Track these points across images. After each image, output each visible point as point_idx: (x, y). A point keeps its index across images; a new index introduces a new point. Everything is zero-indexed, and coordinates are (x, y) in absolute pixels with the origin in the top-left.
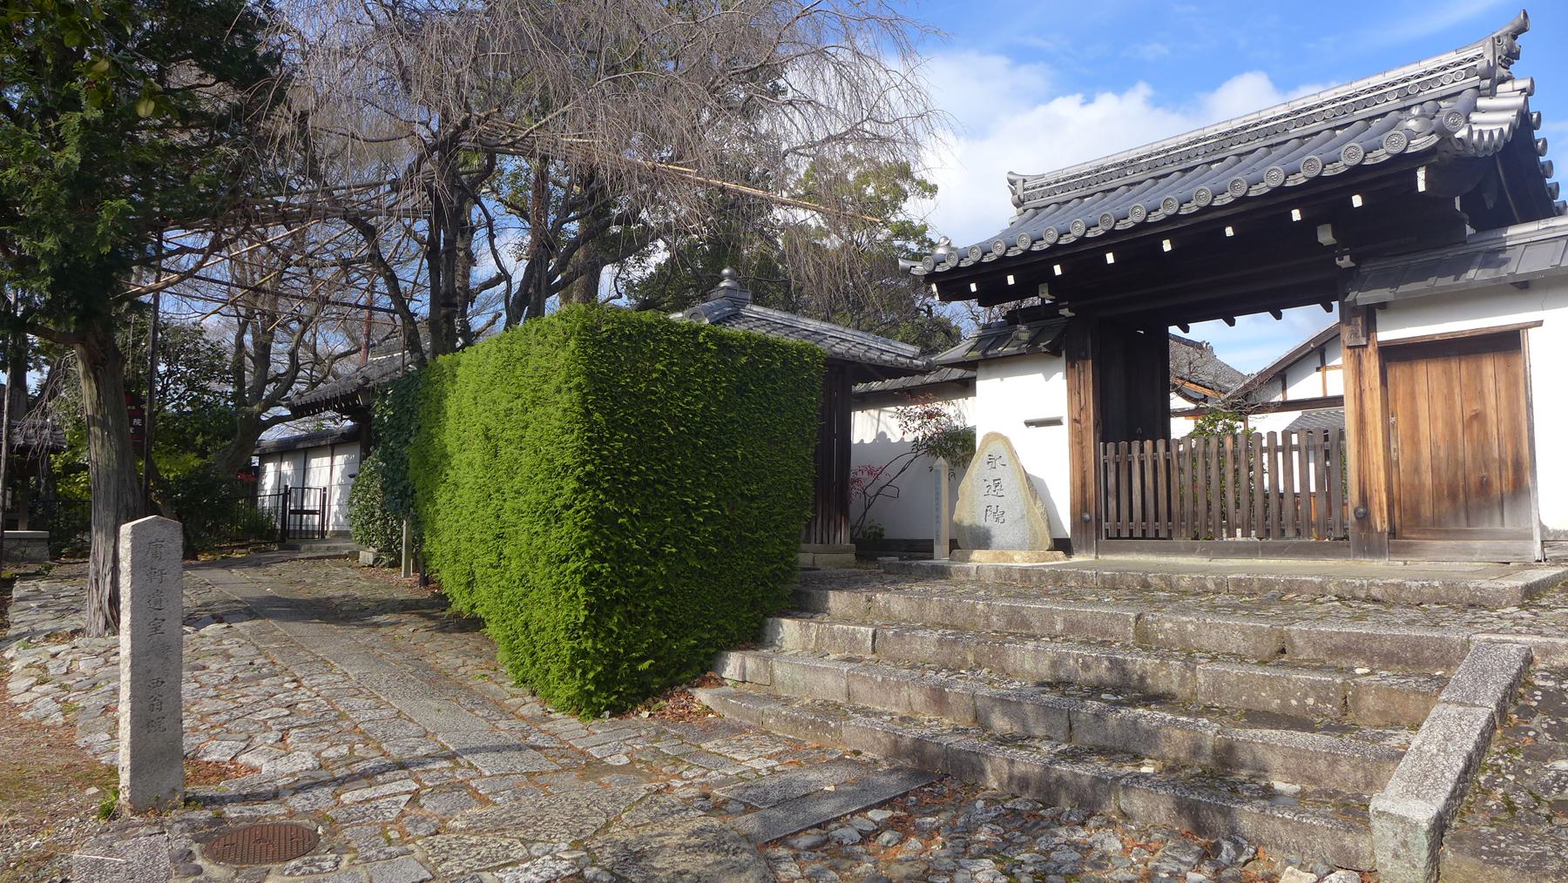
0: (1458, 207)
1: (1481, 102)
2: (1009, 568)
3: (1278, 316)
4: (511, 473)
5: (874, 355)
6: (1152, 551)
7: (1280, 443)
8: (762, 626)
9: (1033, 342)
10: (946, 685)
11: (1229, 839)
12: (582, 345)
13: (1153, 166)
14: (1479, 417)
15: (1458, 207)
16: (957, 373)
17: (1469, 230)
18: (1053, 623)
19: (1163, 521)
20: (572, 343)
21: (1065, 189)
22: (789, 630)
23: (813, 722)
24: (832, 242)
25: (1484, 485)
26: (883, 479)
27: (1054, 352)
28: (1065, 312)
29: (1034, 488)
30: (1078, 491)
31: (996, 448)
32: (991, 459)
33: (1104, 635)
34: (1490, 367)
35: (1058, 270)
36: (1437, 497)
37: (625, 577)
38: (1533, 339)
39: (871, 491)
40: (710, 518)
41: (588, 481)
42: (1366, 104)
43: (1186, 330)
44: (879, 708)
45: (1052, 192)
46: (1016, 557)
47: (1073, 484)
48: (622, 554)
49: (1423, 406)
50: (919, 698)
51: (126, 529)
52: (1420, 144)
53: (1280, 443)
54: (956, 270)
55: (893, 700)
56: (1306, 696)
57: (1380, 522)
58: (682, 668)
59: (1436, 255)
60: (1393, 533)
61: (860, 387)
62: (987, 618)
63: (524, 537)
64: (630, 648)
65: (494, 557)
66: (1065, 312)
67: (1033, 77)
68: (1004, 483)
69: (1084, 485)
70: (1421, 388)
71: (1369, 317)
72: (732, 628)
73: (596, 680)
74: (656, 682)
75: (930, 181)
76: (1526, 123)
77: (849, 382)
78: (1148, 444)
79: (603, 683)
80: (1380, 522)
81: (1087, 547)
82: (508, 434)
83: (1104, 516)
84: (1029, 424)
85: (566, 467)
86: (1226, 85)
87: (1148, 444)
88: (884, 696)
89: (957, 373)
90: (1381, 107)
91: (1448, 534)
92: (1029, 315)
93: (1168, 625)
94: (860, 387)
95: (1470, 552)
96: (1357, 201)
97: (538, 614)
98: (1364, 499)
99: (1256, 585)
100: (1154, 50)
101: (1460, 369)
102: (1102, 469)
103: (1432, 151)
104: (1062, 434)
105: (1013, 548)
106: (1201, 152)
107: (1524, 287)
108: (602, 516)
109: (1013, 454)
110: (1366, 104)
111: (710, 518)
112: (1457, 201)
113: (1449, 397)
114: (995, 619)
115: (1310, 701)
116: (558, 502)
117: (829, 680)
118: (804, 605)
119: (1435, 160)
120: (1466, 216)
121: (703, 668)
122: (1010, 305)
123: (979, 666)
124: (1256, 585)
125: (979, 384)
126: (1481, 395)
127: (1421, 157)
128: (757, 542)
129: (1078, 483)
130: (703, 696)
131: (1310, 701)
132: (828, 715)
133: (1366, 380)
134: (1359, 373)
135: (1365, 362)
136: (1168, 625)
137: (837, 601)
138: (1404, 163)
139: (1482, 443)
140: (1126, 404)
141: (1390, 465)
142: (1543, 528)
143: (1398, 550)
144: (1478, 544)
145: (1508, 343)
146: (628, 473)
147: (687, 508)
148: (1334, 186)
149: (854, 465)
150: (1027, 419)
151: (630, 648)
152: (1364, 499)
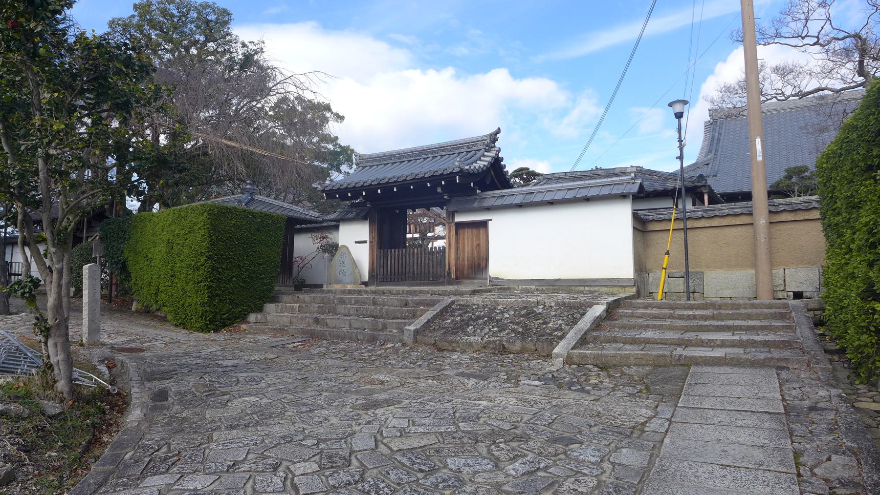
1: (486, 154)
4: (179, 255)
5: (303, 216)
6: (393, 285)
8: (262, 306)
9: (357, 215)
12: (209, 214)
13: (400, 158)
14: (479, 245)
16: (334, 223)
19: (399, 276)
20: (205, 214)
21: (373, 161)
22: (270, 307)
24: (289, 142)
25: (479, 265)
26: (306, 261)
27: (364, 218)
29: (354, 264)
31: (343, 250)
32: (342, 254)
34: (482, 231)
35: (443, 183)
36: (468, 268)
37: (220, 288)
38: (490, 224)
39: (301, 266)
40: (247, 270)
41: (209, 258)
42: (459, 148)
45: (368, 162)
48: (219, 280)
49: (466, 241)
50: (311, 321)
51: (86, 267)
52: (456, 170)
54: (331, 190)
57: (453, 275)
58: (236, 318)
59: (469, 198)
60: (457, 278)
63: (183, 276)
64: (220, 310)
65: (170, 283)
67: (401, 56)
70: (466, 236)
71: (452, 214)
72: (253, 306)
73: (209, 320)
74: (228, 322)
75: (341, 115)
77: (295, 225)
79: (212, 321)
80: (453, 275)
81: (373, 284)
82: (178, 242)
83: (381, 273)
84: (356, 242)
85: (202, 253)
86: (493, 71)
89: (334, 223)
90: (462, 150)
91: (470, 279)
92: (353, 205)
94: (298, 226)
95: (473, 283)
97: (188, 300)
98: (449, 269)
100: (462, 50)
101: (475, 231)
102: (379, 258)
103: (459, 172)
104: (367, 245)
107: (488, 209)
108: (214, 269)
109: (349, 252)
110: (459, 148)
111: (247, 270)
113: (472, 239)
116: (199, 264)
117: (285, 319)
118: (275, 300)
121: (242, 318)
125: (341, 228)
126: (479, 239)
127: (457, 173)
128: (262, 279)
130: (244, 326)
134: (450, 231)
137: (285, 298)
138: (453, 175)
139: (479, 253)
140: (388, 238)
141: (457, 258)
143: (457, 284)
144: (476, 281)
145: (484, 224)
146: (222, 255)
147: (240, 267)
149: (295, 255)
150: (355, 239)
151: (220, 310)
152: (449, 269)
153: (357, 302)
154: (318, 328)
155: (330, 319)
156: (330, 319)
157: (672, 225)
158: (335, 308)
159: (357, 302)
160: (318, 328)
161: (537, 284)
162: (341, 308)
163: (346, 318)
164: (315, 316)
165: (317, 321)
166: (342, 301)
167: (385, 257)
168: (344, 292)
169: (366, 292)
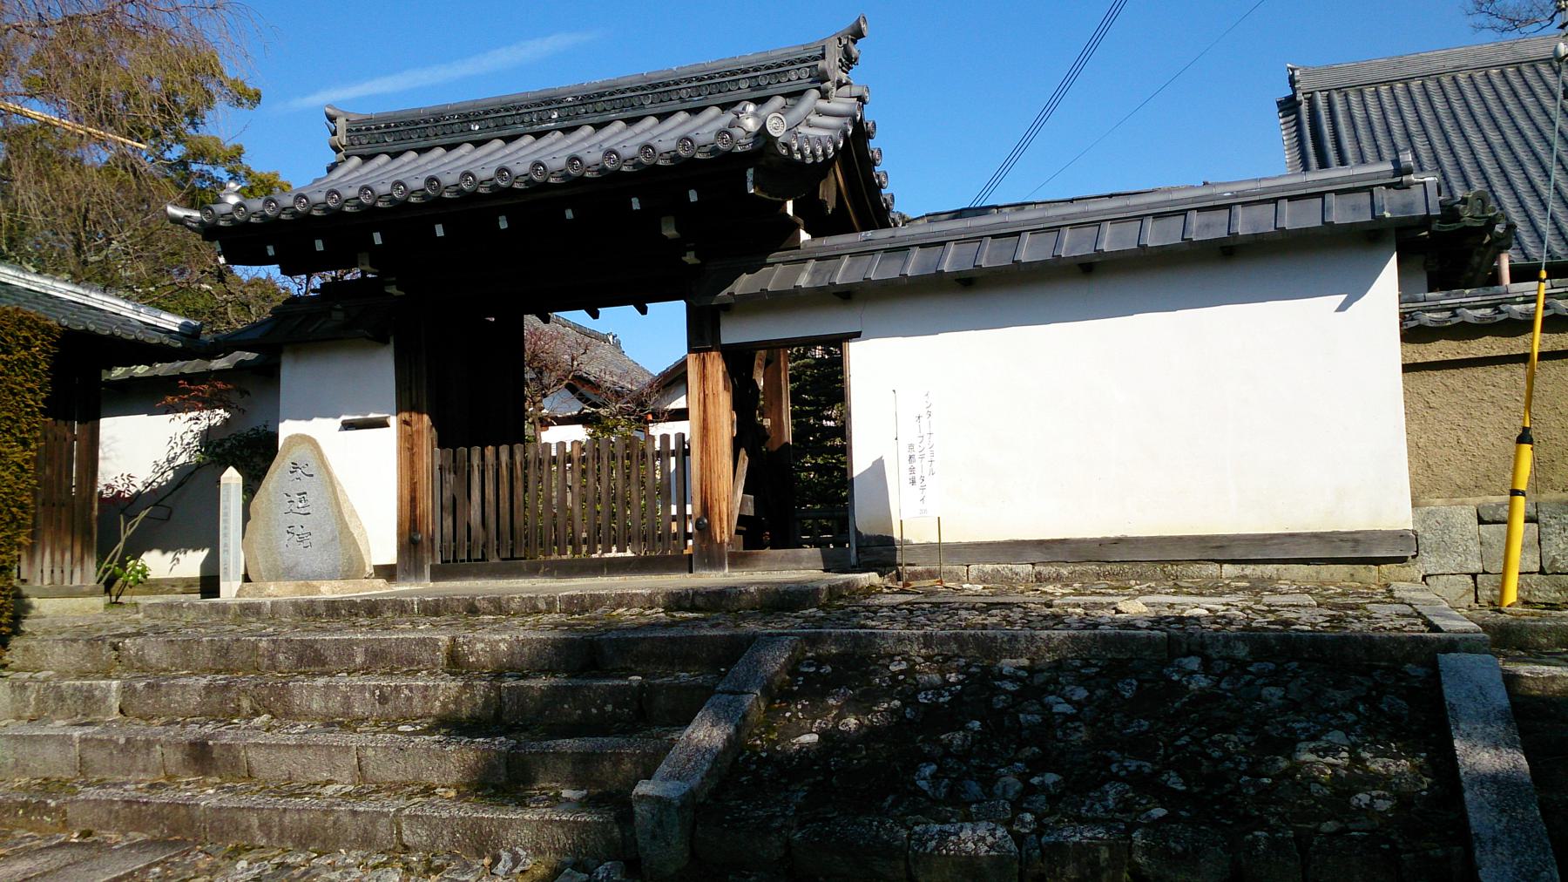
0: (790, 211)
2: (312, 602)
3: (643, 311)
7: (672, 447)
10: (211, 736)
11: (510, 851)
15: (790, 211)
17: (804, 236)
18: (351, 657)
23: (25, 805)
27: (381, 340)
28: (393, 290)
30: (407, 508)
31: (298, 454)
33: (411, 663)
35: (377, 239)
43: (595, 315)
44: (122, 778)
46: (323, 589)
47: (400, 499)
50: (175, 758)
53: (672, 447)
55: (140, 765)
56: (605, 703)
61: (118, 372)
62: (272, 657)
66: (393, 290)
68: (310, 498)
69: (413, 500)
76: (859, 136)
78: (504, 451)
87: (490, 450)
88: (128, 762)
93: (479, 646)
94: (118, 372)
96: (569, 214)
99: (587, 601)
105: (320, 577)
106: (618, 104)
112: (790, 206)
114: (281, 657)
115: (609, 708)
117: (51, 752)
119: (763, 163)
120: (800, 221)
122: (329, 276)
123: (257, 714)
124: (587, 601)
129: (407, 497)
131: (609, 708)
132: (49, 794)
133: (710, 384)
135: (709, 365)
136: (479, 646)
142: (858, 533)
148: (558, 193)
153: (378, 659)
154: (209, 797)
155: (253, 738)
156: (253, 738)
157: (1538, 341)
158: (282, 693)
159: (378, 659)
160: (209, 797)
161: (1037, 556)
162: (311, 693)
163: (337, 738)
164: (194, 731)
165: (201, 756)
166: (311, 660)
167: (461, 471)
168: (308, 611)
169: (401, 607)
